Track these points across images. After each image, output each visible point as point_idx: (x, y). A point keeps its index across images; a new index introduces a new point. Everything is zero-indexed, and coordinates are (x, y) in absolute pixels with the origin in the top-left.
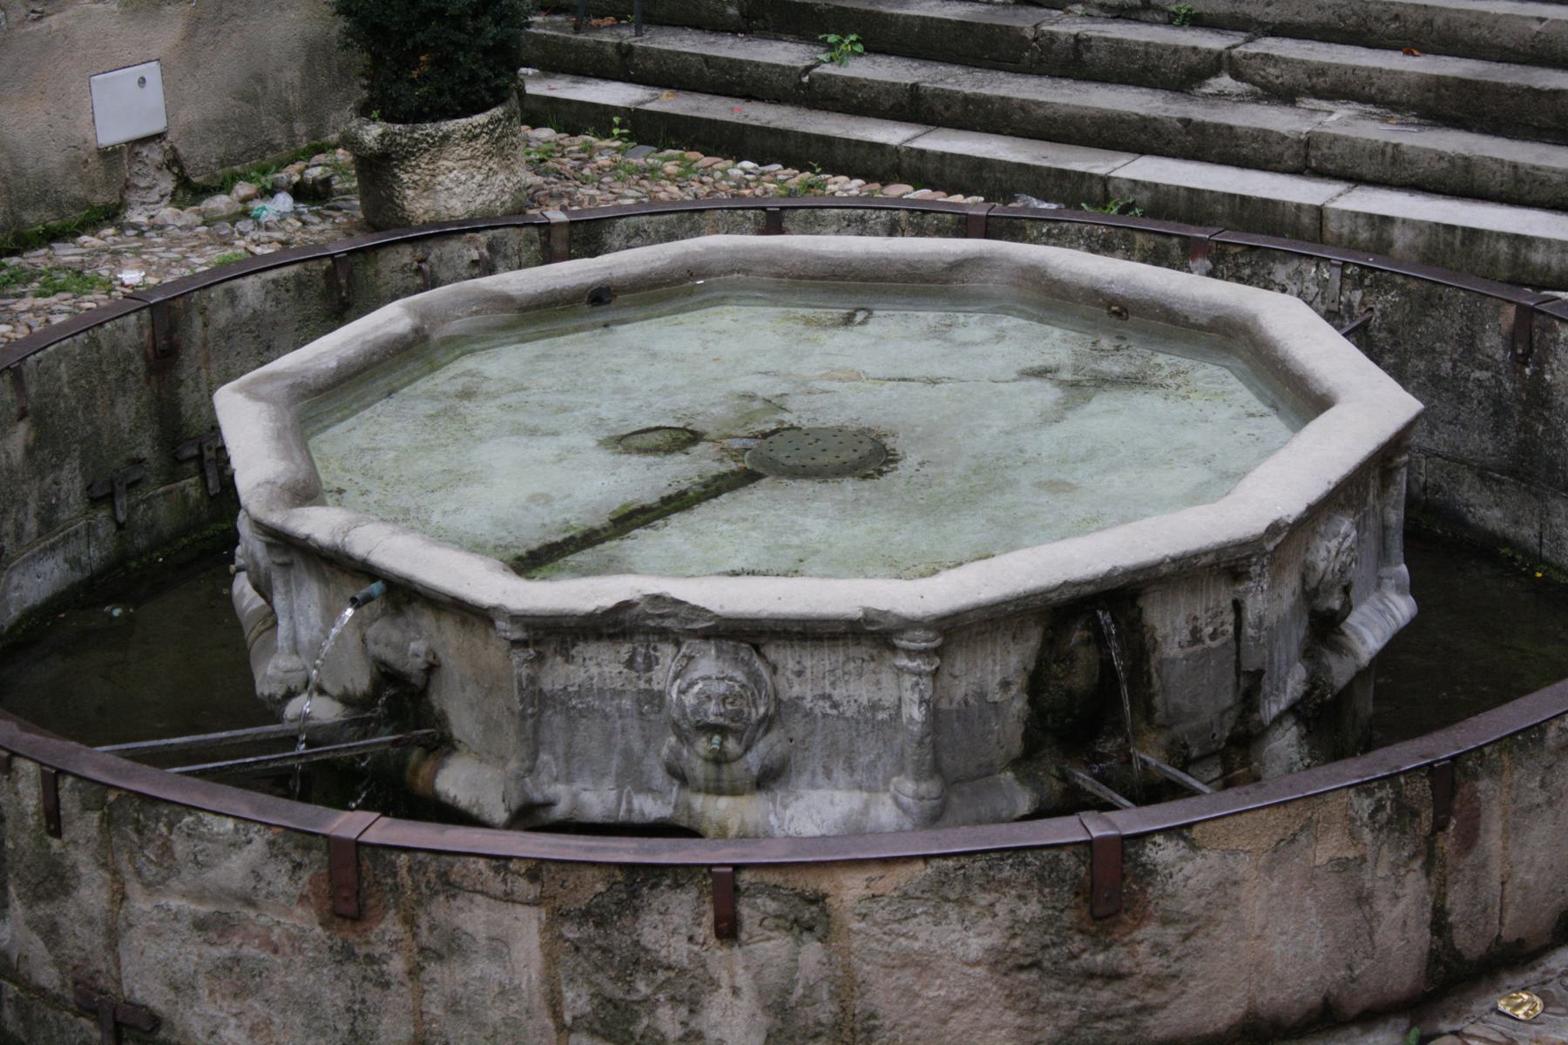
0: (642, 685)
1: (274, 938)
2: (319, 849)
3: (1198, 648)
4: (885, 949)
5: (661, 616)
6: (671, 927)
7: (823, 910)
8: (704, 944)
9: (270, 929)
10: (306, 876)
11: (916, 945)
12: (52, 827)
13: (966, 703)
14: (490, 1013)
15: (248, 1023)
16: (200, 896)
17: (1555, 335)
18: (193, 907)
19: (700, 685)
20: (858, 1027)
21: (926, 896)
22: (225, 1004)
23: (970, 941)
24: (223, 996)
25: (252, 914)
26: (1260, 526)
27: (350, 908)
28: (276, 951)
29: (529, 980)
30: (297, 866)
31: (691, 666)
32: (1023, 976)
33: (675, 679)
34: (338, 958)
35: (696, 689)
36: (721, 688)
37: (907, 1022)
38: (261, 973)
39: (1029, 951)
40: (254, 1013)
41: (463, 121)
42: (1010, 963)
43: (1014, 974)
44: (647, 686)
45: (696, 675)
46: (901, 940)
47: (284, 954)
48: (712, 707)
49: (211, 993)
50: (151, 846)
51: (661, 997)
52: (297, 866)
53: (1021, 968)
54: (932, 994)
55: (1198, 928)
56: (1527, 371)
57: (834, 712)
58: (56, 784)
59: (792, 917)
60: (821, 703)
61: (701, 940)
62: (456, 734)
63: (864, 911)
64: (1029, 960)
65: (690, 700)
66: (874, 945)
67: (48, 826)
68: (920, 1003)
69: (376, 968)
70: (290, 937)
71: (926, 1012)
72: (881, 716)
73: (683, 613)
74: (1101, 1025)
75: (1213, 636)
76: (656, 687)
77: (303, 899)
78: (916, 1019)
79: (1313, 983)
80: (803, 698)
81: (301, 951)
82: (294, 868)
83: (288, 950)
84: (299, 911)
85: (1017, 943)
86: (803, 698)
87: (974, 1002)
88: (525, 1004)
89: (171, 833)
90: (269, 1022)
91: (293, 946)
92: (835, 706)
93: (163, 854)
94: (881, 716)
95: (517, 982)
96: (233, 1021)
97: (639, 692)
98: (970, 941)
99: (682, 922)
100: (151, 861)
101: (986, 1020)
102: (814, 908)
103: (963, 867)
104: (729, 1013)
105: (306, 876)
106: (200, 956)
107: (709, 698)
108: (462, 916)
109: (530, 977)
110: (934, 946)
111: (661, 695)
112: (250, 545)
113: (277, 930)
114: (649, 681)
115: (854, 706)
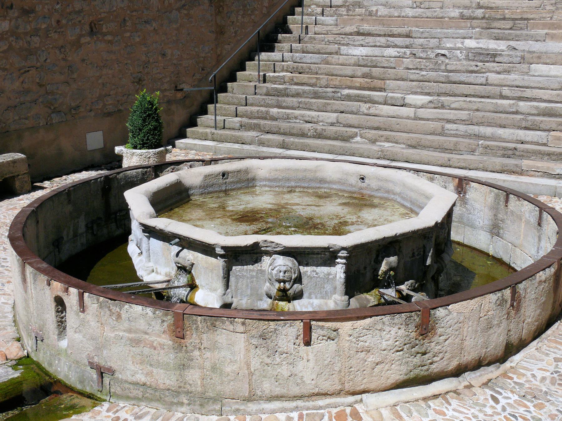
0: (259, 268)
1: (155, 345)
2: (171, 315)
3: (414, 258)
4: (357, 346)
5: (266, 247)
6: (288, 340)
7: (338, 333)
8: (299, 345)
9: (153, 342)
10: (165, 324)
11: (367, 344)
12: (81, 310)
13: (355, 273)
14: (226, 369)
15: (145, 372)
16: (130, 331)
17: (470, 185)
18: (127, 335)
19: (278, 267)
20: (346, 371)
21: (370, 328)
22: (137, 366)
23: (383, 343)
24: (137, 364)
25: (147, 337)
26: (432, 223)
27: (180, 335)
28: (155, 349)
29: (240, 358)
30: (163, 321)
31: (275, 262)
32: (398, 353)
33: (270, 266)
34: (176, 351)
35: (276, 269)
36: (284, 269)
37: (362, 369)
38: (150, 356)
39: (401, 345)
40: (147, 369)
41: (153, 150)
42: (394, 350)
43: (395, 353)
44: (260, 268)
45: (276, 265)
46: (362, 343)
47: (158, 350)
48: (282, 274)
49: (133, 362)
50: (114, 315)
51: (284, 363)
52: (163, 321)
53: (398, 351)
54: (370, 360)
55: (449, 337)
56: (461, 195)
57: (317, 276)
58: (83, 294)
59: (328, 336)
60: (313, 273)
61: (298, 344)
62: (197, 284)
63: (351, 334)
64: (401, 348)
65: (274, 272)
66: (354, 345)
67: (80, 310)
68: (366, 363)
69: (188, 354)
70: (160, 344)
71: (368, 366)
72: (331, 277)
73: (273, 245)
74: (420, 368)
75: (417, 255)
76: (263, 269)
77: (164, 332)
78: (365, 368)
79: (477, 353)
80: (307, 272)
81: (164, 349)
82: (162, 322)
83: (159, 348)
84: (163, 336)
85: (397, 343)
86: (307, 272)
87: (383, 362)
88: (239, 366)
89: (121, 311)
90: (152, 372)
91: (161, 347)
92: (317, 274)
93: (118, 318)
94: (331, 277)
95: (236, 358)
96: (140, 372)
97: (258, 270)
98: (383, 343)
99: (292, 338)
100: (114, 320)
101: (387, 367)
102: (335, 333)
103: (382, 319)
104: (306, 367)
105: (165, 324)
106: (130, 351)
107: (280, 272)
108: (218, 337)
109: (240, 357)
110: (372, 345)
111: (264, 271)
112: (135, 228)
113: (156, 342)
114: (261, 267)
115: (323, 274)
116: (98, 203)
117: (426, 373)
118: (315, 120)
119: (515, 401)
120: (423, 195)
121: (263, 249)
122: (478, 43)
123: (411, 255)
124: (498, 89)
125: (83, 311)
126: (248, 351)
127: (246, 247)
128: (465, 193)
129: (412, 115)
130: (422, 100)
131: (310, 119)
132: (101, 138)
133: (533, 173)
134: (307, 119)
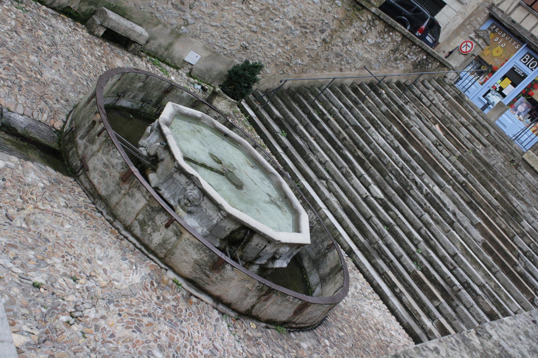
10: (123, 170)
16: (108, 160)
26: (278, 239)
27: (124, 179)
30: (123, 168)
36: (194, 196)
48: (191, 197)
52: (123, 168)
65: (189, 194)
77: (120, 173)
105: (123, 170)
116: (156, 94)
117: (202, 285)
118: (315, 152)
119: (31, 22)
120: (399, 273)
121: (67, 127)
122: (441, 193)
123: (256, 244)
124: (421, 224)
125: (98, 136)
126: (142, 209)
127: (187, 172)
128: (329, 251)
129: (364, 196)
130: (378, 193)
131: (313, 149)
132: (197, 60)
133: (386, 281)
134: (311, 147)
